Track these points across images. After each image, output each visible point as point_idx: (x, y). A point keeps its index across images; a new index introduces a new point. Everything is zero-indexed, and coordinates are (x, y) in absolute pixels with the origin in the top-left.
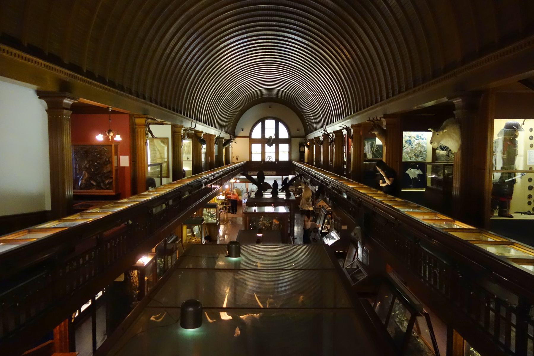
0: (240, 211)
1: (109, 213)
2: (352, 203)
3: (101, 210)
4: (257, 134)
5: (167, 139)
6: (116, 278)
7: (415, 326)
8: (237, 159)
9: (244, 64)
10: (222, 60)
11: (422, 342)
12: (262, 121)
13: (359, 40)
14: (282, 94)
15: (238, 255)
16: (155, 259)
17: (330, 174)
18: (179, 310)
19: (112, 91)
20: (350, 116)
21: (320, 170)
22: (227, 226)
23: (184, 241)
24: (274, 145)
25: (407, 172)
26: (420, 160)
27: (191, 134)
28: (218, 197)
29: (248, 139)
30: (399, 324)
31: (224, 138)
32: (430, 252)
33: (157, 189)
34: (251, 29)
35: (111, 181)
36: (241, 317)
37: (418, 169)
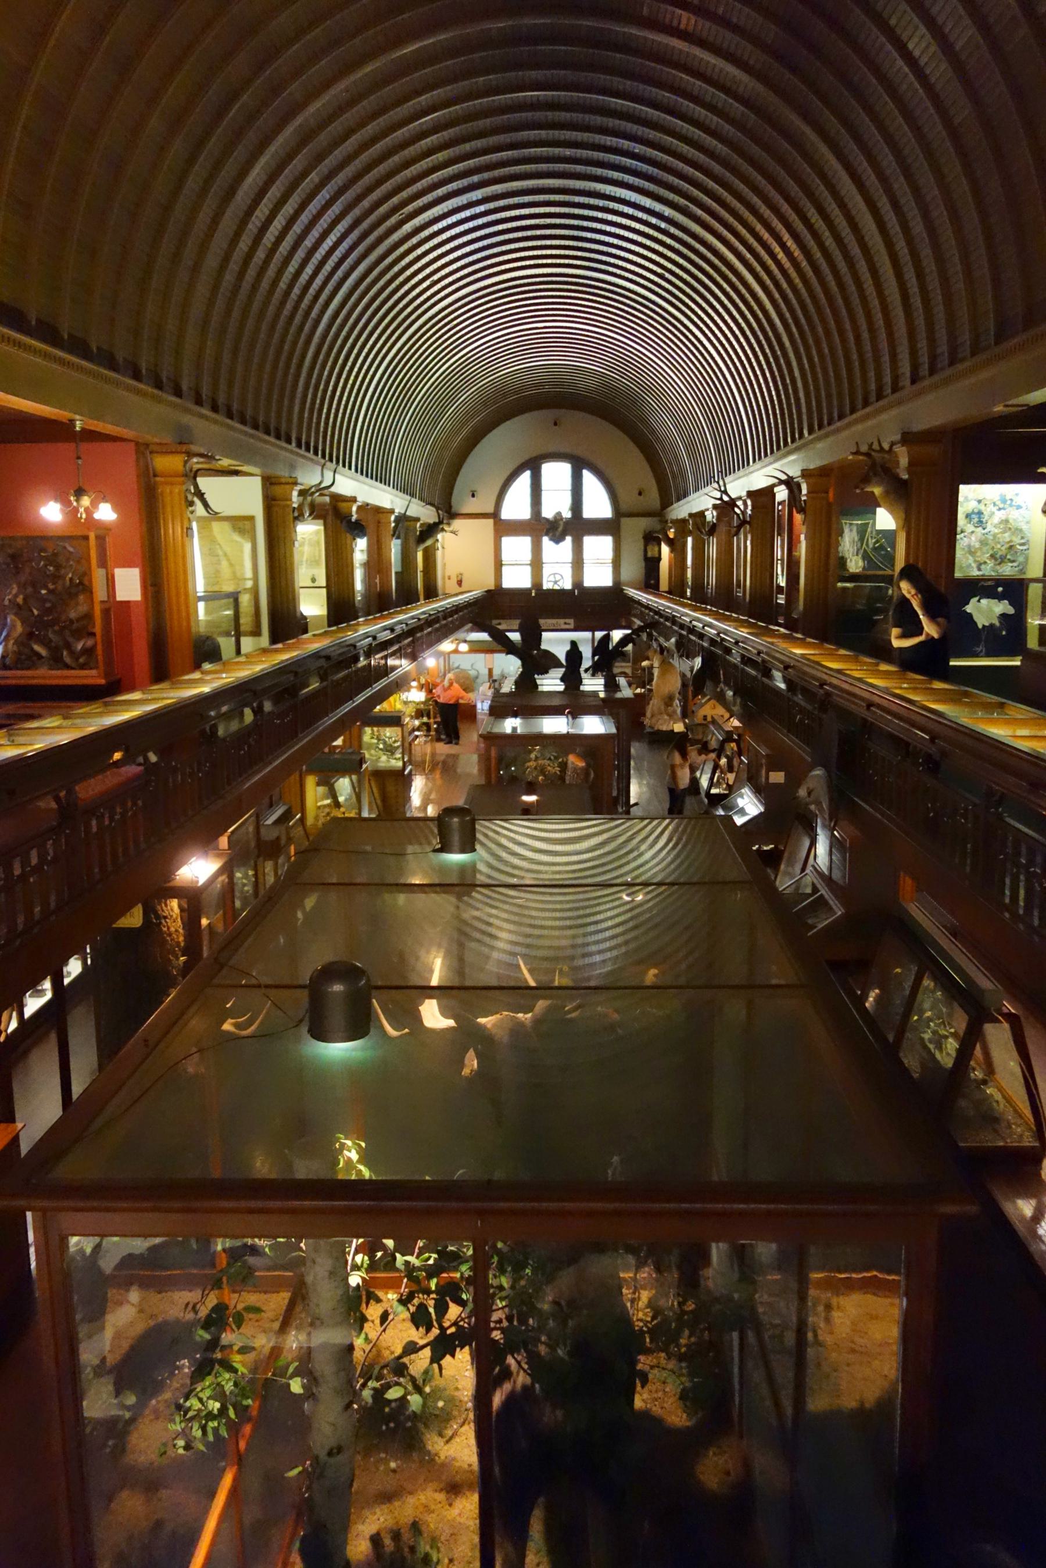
0: (471, 737)
1: (91, 729)
2: (803, 703)
3: (66, 723)
4: (516, 505)
5: (251, 519)
6: (118, 918)
7: (978, 1050)
8: (460, 583)
9: (473, 287)
10: (408, 273)
11: (998, 1096)
12: (534, 465)
13: (830, 199)
14: (593, 383)
15: (468, 845)
16: (227, 869)
17: (736, 620)
18: (304, 996)
19: (80, 369)
20: (798, 443)
21: (705, 609)
22: (434, 780)
23: (310, 821)
24: (569, 539)
25: (969, 609)
26: (1007, 570)
27: (323, 505)
28: (404, 696)
29: (491, 521)
30: (931, 1046)
31: (418, 519)
32: (1031, 833)
33: (227, 666)
34: (496, 173)
35: (90, 643)
36: (482, 1020)
37: (1000, 597)
